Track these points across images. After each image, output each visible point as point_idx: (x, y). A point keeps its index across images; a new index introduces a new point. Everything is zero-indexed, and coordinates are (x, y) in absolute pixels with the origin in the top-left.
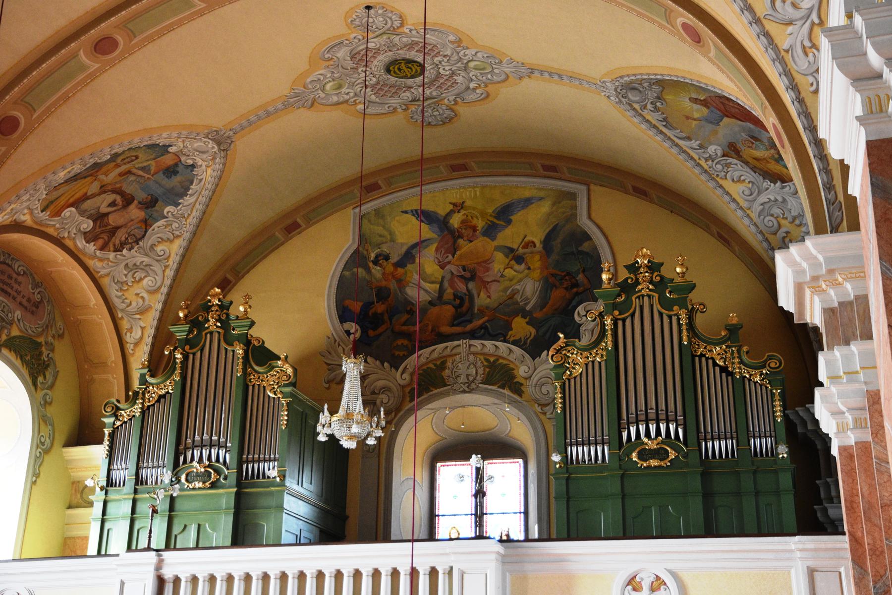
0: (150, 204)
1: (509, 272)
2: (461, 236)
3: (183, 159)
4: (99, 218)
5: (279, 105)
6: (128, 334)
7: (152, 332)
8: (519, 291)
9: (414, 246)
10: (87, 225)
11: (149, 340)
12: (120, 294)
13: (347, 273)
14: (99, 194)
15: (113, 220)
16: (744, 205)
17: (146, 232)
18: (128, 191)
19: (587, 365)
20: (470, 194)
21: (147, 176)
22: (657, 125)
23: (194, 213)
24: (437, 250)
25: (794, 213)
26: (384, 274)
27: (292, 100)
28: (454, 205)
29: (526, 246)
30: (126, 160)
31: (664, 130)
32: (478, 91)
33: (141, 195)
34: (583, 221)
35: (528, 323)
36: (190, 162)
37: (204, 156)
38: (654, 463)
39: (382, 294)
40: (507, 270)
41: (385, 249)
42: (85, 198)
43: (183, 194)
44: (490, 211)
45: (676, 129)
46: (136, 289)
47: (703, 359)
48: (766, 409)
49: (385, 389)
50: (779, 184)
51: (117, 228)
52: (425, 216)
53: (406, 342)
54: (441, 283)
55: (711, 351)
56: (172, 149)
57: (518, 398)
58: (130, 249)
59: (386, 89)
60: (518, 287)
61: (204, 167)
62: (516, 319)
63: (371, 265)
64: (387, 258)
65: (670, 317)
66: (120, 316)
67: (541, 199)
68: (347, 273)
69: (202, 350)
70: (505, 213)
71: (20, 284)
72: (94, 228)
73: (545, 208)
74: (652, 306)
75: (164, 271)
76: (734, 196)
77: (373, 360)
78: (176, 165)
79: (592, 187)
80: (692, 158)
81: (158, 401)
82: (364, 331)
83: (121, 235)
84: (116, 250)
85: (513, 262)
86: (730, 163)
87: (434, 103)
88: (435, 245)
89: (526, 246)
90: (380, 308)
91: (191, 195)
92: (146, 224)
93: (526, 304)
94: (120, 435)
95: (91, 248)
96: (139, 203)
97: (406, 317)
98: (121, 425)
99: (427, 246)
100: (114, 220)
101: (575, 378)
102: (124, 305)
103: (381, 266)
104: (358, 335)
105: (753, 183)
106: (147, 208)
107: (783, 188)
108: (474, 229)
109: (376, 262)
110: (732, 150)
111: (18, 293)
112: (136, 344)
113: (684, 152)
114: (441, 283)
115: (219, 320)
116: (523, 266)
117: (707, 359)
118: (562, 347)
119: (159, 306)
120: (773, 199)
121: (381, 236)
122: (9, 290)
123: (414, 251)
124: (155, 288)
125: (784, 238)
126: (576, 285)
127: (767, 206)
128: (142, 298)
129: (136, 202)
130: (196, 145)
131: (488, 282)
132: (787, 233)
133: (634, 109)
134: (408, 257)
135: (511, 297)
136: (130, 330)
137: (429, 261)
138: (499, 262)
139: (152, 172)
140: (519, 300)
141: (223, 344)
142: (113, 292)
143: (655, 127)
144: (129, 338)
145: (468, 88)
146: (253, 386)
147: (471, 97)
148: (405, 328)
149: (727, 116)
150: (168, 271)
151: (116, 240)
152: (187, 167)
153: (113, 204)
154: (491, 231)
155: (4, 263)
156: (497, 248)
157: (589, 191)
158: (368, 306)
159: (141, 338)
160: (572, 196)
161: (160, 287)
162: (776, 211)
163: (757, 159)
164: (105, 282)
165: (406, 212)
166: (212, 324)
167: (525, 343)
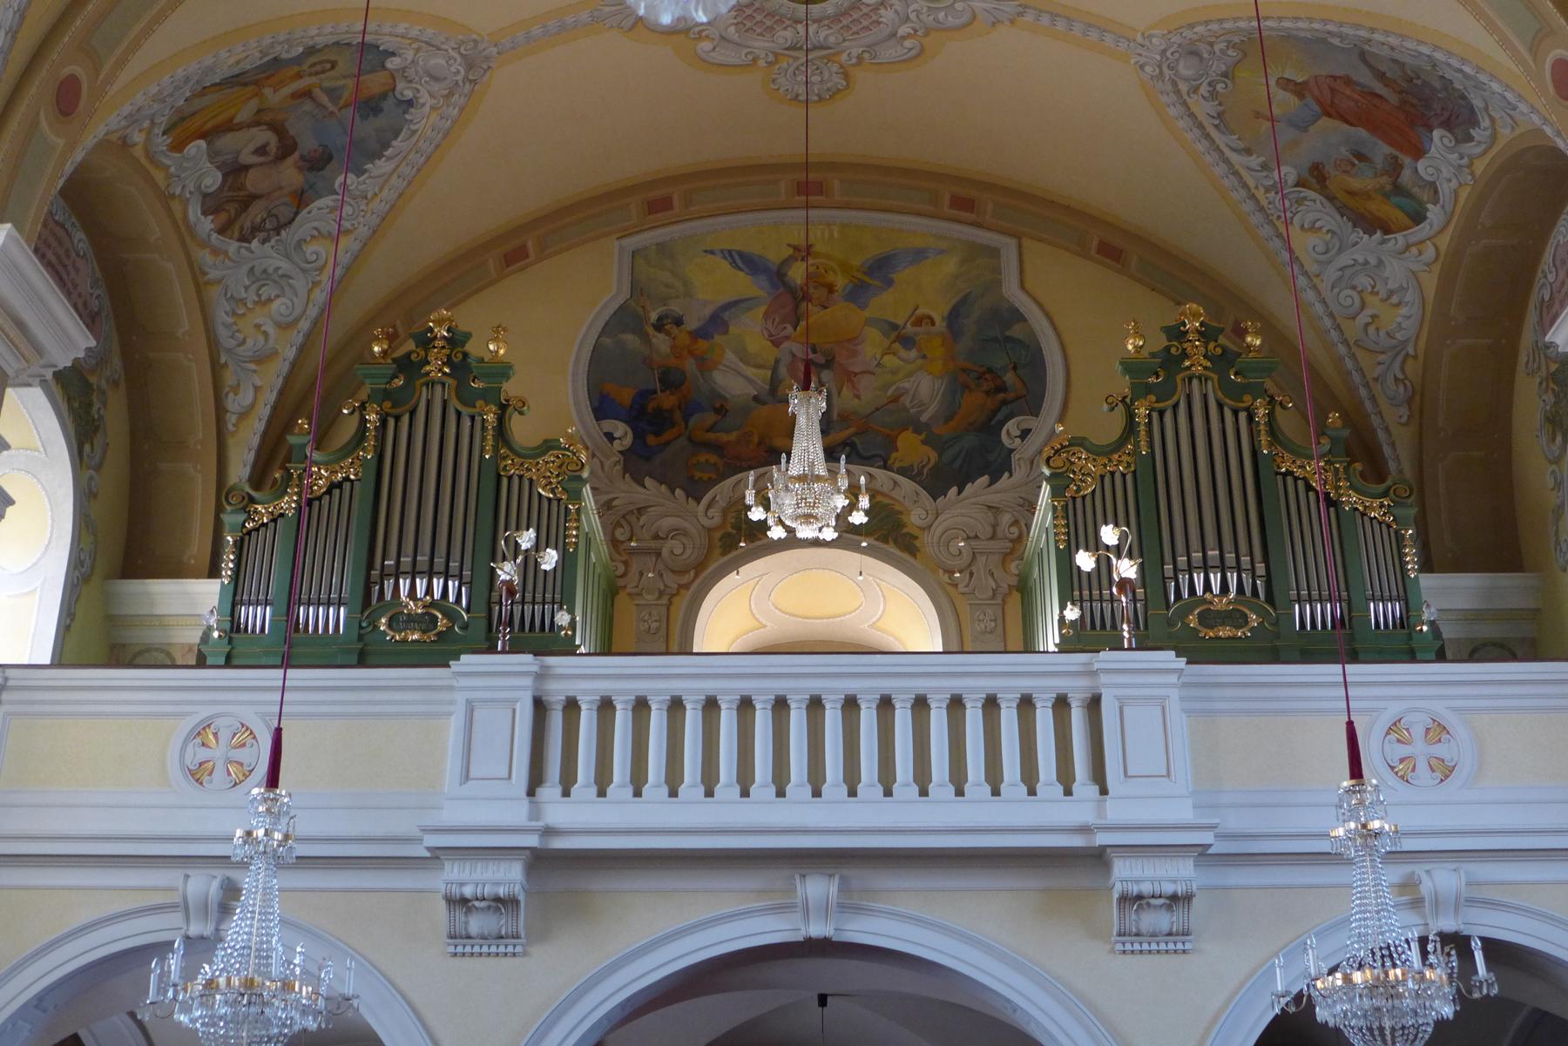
0: (318, 163)
1: (890, 361)
2: (806, 297)
3: (400, 86)
4: (234, 171)
5: (584, 16)
6: (231, 395)
7: (273, 397)
8: (907, 391)
9: (727, 307)
10: (213, 180)
11: (264, 411)
12: (230, 320)
13: (607, 341)
14: (249, 126)
15: (253, 181)
16: (1312, 268)
17: (297, 214)
18: (292, 132)
19: (1102, 477)
20: (836, 233)
21: (331, 108)
22: (1205, 123)
23: (385, 192)
24: (766, 316)
25: (1392, 285)
26: (673, 347)
27: (607, 9)
28: (796, 248)
29: (918, 322)
30: (318, 68)
31: (1214, 134)
32: (908, 43)
33: (308, 144)
34: (1011, 290)
35: (924, 442)
36: (409, 94)
37: (436, 87)
38: (1225, 632)
39: (670, 379)
40: (887, 358)
41: (676, 307)
42: (229, 127)
43: (376, 155)
44: (856, 262)
45: (1232, 133)
46: (259, 317)
47: (1289, 479)
48: (1391, 567)
49: (677, 533)
50: (1378, 234)
51: (254, 197)
52: (749, 263)
53: (713, 458)
54: (775, 370)
55: (1303, 467)
56: (392, 63)
57: (911, 560)
58: (264, 242)
59: (759, 18)
60: (906, 385)
61: (427, 108)
62: (904, 434)
63: (650, 330)
64: (678, 322)
65: (1235, 413)
66: (223, 360)
67: (942, 252)
68: (607, 341)
69: (413, 413)
70: (881, 269)
71: (77, 270)
72: (221, 188)
73: (950, 265)
74: (1205, 397)
75: (310, 291)
76: (1298, 253)
77: (655, 484)
78: (384, 96)
79: (1026, 242)
80: (1245, 186)
81: (329, 492)
82: (639, 436)
83: (256, 212)
84: (243, 239)
85: (897, 346)
86: (1305, 198)
87: (822, 58)
88: (763, 309)
89: (918, 322)
90: (668, 400)
91: (389, 159)
92: (301, 199)
93: (922, 412)
94: (256, 545)
95: (206, 225)
96: (302, 157)
97: (711, 418)
98: (257, 530)
99: (750, 309)
100: (254, 181)
101: (1084, 497)
102: (233, 343)
103: (668, 333)
104: (628, 441)
105: (1334, 233)
106: (311, 169)
107: (1383, 242)
108: (830, 289)
109: (659, 326)
110: (1317, 177)
111: (75, 286)
112: (243, 415)
113: (1236, 173)
114: (775, 370)
115: (449, 362)
116: (913, 353)
117: (1296, 479)
118: (1063, 447)
119: (291, 353)
120: (1361, 260)
121: (667, 286)
122: (65, 276)
123: (726, 315)
124: (290, 319)
125: (1367, 325)
126: (1002, 388)
127: (1348, 272)
128: (265, 334)
129: (297, 155)
130: (433, 62)
131: (856, 374)
132: (1374, 317)
133: (1178, 92)
134: (717, 322)
135: (895, 399)
136: (236, 389)
137: (751, 331)
138: (873, 344)
139: (342, 102)
140: (908, 405)
141: (454, 404)
142: (221, 315)
143: (1201, 126)
144: (234, 404)
145: (894, 35)
146: (510, 478)
147: (890, 53)
148: (712, 436)
149: (1330, 116)
150: (317, 292)
151: (247, 221)
152: (400, 103)
153: (261, 150)
154: (858, 293)
155: (62, 226)
156: (869, 322)
157: (1020, 246)
158: (644, 395)
159: (252, 406)
160: (994, 253)
161: (297, 320)
162: (1363, 281)
163: (1351, 193)
164: (215, 292)
165: (712, 252)
166: (435, 367)
167: (920, 473)
